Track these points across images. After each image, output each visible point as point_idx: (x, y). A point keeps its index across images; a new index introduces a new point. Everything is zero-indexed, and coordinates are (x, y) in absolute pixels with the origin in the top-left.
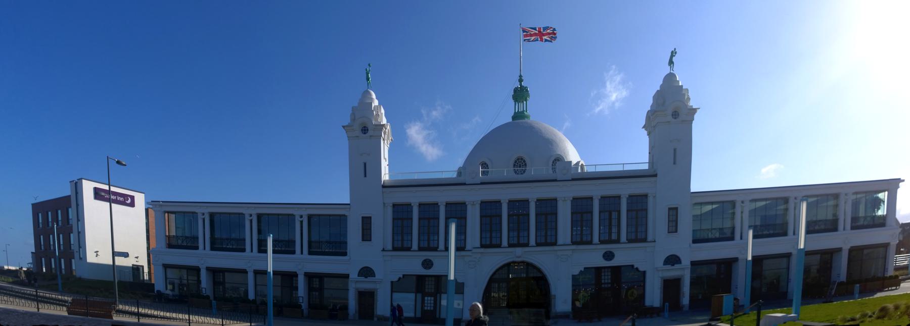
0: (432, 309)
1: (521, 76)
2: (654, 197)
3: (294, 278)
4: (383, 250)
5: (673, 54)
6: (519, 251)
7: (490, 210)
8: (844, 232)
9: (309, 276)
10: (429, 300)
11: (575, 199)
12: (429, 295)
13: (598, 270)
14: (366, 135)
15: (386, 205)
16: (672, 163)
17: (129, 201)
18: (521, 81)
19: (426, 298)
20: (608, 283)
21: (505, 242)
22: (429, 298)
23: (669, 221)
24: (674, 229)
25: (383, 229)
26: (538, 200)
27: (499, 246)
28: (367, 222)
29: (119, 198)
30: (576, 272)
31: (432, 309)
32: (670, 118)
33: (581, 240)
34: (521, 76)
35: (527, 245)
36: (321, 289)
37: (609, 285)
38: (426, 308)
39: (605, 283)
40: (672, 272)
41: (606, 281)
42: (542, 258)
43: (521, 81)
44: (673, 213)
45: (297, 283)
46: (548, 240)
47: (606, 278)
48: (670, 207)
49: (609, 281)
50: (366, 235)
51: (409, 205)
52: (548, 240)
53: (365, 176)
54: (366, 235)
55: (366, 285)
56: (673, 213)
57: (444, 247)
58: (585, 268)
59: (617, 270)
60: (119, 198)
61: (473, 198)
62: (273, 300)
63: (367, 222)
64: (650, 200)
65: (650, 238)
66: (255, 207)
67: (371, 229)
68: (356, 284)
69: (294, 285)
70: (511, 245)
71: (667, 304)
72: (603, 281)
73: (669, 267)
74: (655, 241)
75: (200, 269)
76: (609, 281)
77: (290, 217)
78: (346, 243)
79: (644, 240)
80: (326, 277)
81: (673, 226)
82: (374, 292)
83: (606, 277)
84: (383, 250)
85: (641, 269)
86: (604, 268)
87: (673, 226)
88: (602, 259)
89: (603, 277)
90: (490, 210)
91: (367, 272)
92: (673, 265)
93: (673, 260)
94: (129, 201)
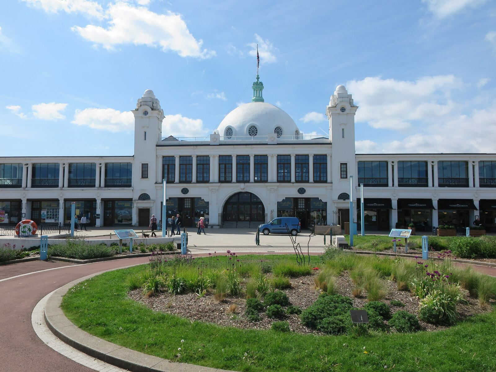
1: (258, 76)
2: (331, 156)
3: (94, 202)
4: (156, 183)
6: (242, 185)
7: (225, 161)
9: (105, 201)
11: (279, 156)
13: (296, 200)
14: (146, 116)
15: (158, 157)
16: (345, 130)
18: (258, 78)
21: (234, 179)
23: (341, 171)
24: (345, 176)
25: (156, 171)
26: (255, 155)
27: (230, 182)
28: (145, 168)
30: (280, 200)
32: (339, 111)
33: (283, 179)
34: (258, 76)
35: (248, 182)
36: (113, 208)
39: (300, 208)
40: (344, 204)
42: (258, 190)
43: (258, 78)
44: (344, 167)
45: (96, 206)
46: (262, 179)
47: (301, 205)
49: (304, 207)
50: (145, 175)
51: (173, 157)
52: (262, 179)
53: (145, 139)
54: (145, 175)
55: (144, 204)
56: (344, 167)
57: (196, 180)
58: (286, 198)
59: (307, 200)
61: (214, 154)
63: (145, 168)
64: (329, 158)
65: (329, 180)
66: (67, 159)
67: (147, 171)
68: (138, 205)
69: (94, 207)
70: (238, 182)
72: (299, 207)
73: (342, 201)
74: (332, 183)
75: (22, 200)
77: (93, 166)
78: (131, 179)
79: (326, 182)
80: (116, 200)
81: (344, 173)
82: (149, 209)
83: (301, 204)
84: (156, 183)
85: (324, 201)
86: (301, 198)
87: (344, 173)
89: (299, 204)
90: (225, 161)
91: (144, 197)
93: (344, 196)
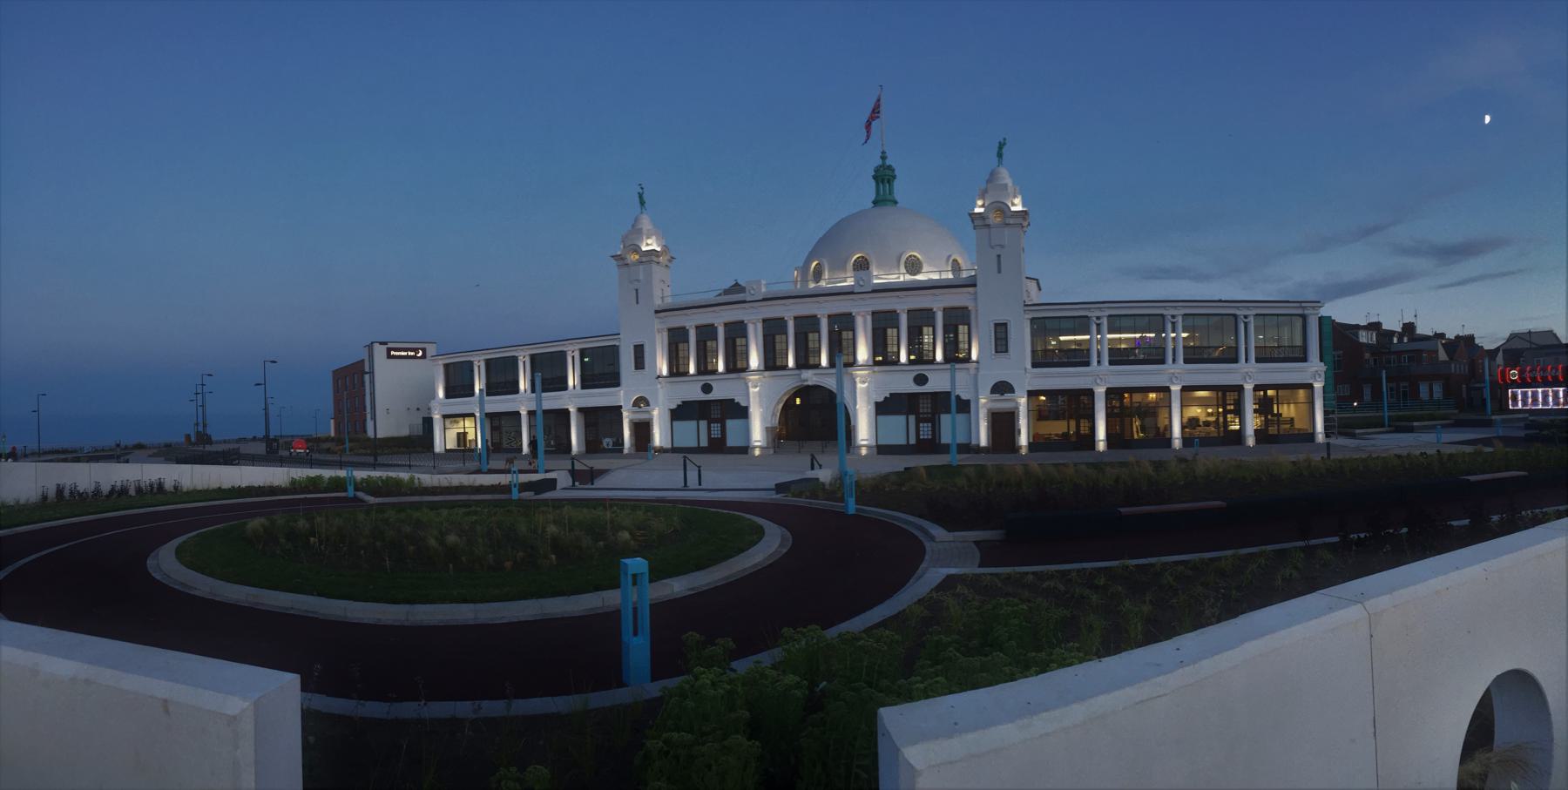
0: (720, 436)
1: (883, 152)
5: (1001, 146)
8: (1174, 366)
10: (716, 428)
12: (716, 421)
17: (420, 354)
18: (883, 158)
19: (712, 425)
20: (928, 413)
22: (716, 425)
29: (410, 353)
31: (720, 436)
34: (883, 152)
37: (929, 416)
38: (713, 436)
41: (925, 411)
43: (883, 158)
48: (997, 322)
49: (929, 411)
54: (639, 363)
60: (410, 353)
62: (717, 362)
71: (1481, 371)
76: (929, 411)
88: (912, 384)
92: (1002, 394)
94: (420, 354)
